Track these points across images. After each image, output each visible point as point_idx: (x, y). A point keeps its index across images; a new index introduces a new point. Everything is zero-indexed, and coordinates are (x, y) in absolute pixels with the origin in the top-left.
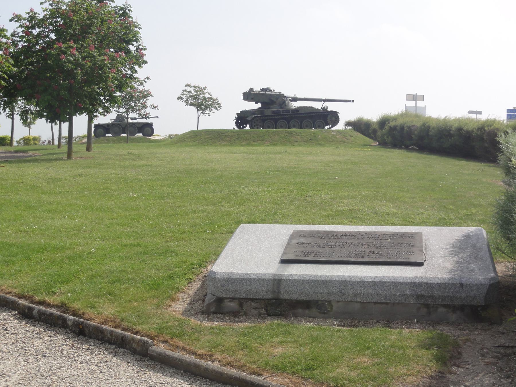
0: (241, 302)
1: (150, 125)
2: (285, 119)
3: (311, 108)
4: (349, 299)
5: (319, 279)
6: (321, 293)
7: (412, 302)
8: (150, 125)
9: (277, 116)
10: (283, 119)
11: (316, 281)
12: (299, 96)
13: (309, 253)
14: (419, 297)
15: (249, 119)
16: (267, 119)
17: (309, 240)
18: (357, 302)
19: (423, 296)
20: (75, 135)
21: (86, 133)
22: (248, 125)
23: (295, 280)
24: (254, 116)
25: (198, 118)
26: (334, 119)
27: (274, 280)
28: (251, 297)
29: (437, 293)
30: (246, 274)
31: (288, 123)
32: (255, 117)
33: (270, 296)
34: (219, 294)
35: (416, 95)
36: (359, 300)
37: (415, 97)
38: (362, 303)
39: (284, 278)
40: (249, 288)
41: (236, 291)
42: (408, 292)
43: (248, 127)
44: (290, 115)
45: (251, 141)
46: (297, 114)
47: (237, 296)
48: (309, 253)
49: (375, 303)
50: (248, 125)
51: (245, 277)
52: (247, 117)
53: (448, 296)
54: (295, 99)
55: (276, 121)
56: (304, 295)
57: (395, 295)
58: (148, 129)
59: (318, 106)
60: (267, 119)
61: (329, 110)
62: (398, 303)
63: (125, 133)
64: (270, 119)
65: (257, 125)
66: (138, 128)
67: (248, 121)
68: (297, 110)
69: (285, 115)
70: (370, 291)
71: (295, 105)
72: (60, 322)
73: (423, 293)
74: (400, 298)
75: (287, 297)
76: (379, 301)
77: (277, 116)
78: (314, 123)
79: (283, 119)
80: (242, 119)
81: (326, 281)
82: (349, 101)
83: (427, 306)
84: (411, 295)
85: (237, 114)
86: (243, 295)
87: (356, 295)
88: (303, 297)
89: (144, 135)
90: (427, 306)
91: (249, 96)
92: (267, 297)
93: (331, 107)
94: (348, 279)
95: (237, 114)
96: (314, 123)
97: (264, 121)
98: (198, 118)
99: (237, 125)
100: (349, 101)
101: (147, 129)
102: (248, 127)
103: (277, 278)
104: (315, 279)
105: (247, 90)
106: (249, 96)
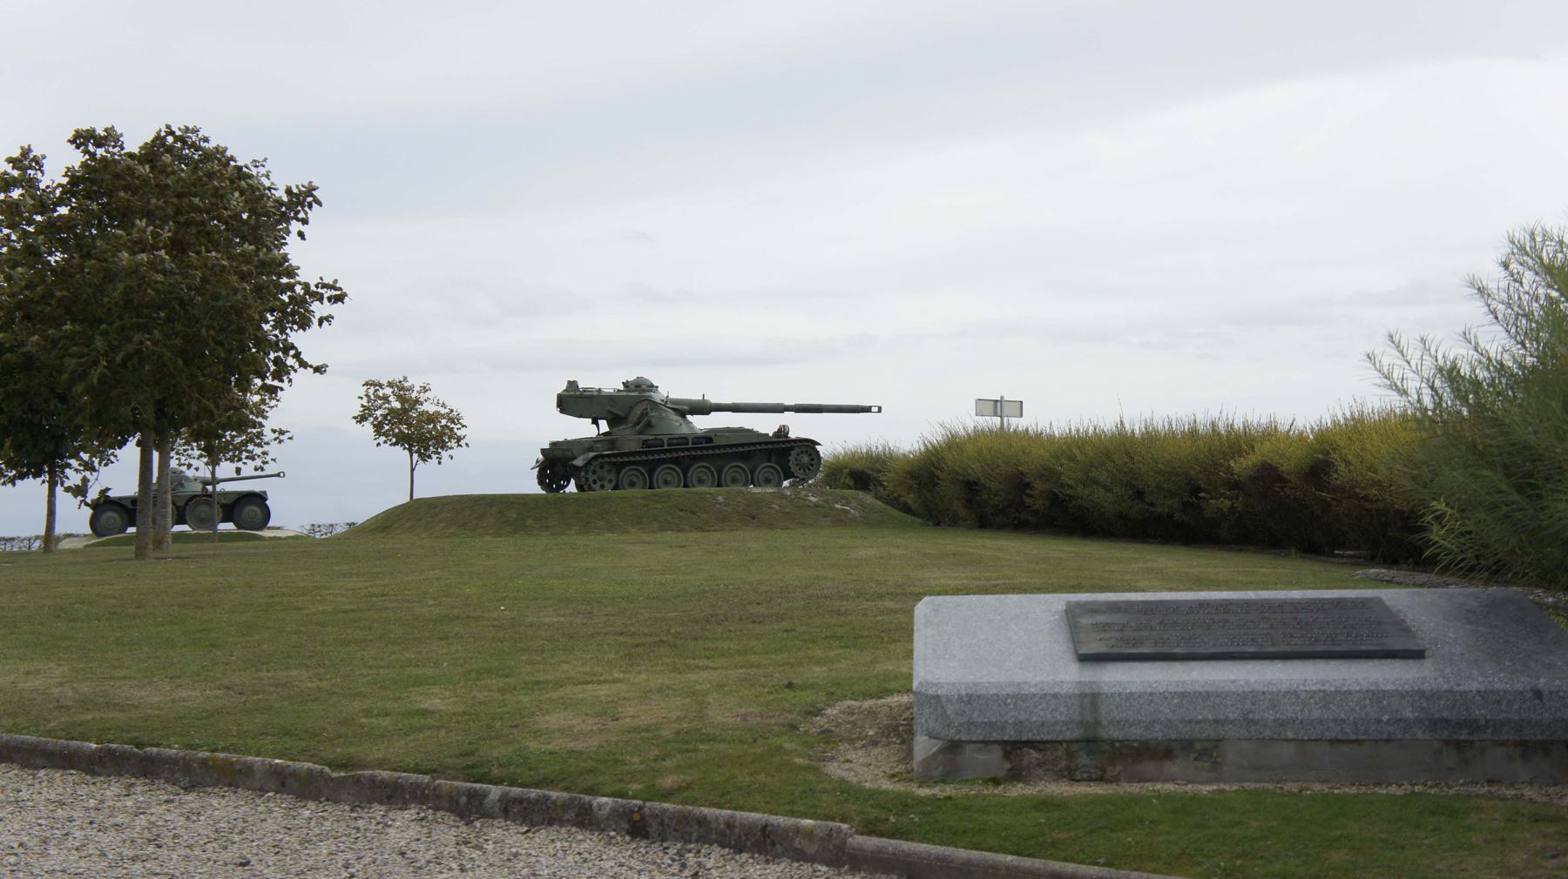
0: (1012, 748)
1: (259, 499)
2: (676, 461)
3: (741, 430)
4: (1268, 733)
5: (1189, 688)
6: (1199, 722)
7: (1420, 735)
8: (259, 499)
9: (652, 453)
10: (671, 461)
11: (1183, 695)
12: (714, 399)
13: (1137, 642)
14: (1436, 724)
15: (579, 462)
16: (629, 463)
17: (1118, 618)
18: (1287, 740)
19: (1447, 721)
20: (60, 529)
21: (42, 532)
22: (573, 482)
23: (1131, 694)
24: (592, 454)
25: (413, 470)
26: (806, 459)
27: (1083, 695)
28: (1030, 736)
29: (1479, 713)
30: (1011, 684)
31: (685, 473)
32: (595, 458)
33: (1077, 733)
34: (952, 733)
35: (1001, 401)
36: (1290, 735)
37: (997, 406)
38: (1299, 741)
39: (1106, 689)
40: (1023, 717)
41: (992, 725)
42: (1409, 714)
43: (572, 488)
44: (689, 449)
45: (582, 518)
46: (707, 449)
47: (995, 736)
48: (1137, 642)
49: (1332, 742)
50: (573, 482)
51: (1009, 690)
52: (574, 458)
53: (1509, 721)
54: (703, 408)
55: (652, 467)
56: (1157, 727)
57: (1379, 721)
58: (251, 510)
59: (766, 425)
60: (629, 463)
61: (792, 435)
62: (1388, 741)
63: (184, 522)
64: (634, 463)
65: (601, 479)
66: (223, 506)
67: (576, 467)
68: (708, 438)
69: (677, 451)
70: (1316, 714)
71: (700, 423)
72: (571, 815)
73: (1446, 714)
74: (1391, 728)
75: (1116, 734)
76: (1340, 736)
77: (652, 453)
78: (752, 473)
79: (671, 461)
80: (556, 463)
81: (1208, 694)
82: (867, 410)
83: (1459, 746)
84: (1418, 721)
85: (543, 451)
86: (1011, 734)
87: (1281, 725)
88: (1157, 734)
89: (238, 526)
90: (1459, 746)
91: (573, 401)
92: (1068, 736)
93: (800, 426)
94: (1260, 688)
95: (543, 451)
96: (752, 473)
97: (619, 467)
98: (413, 470)
99: (541, 482)
100: (867, 410)
101: (249, 509)
102: (572, 488)
103: (1087, 690)
104: (1180, 689)
105: (561, 387)
106: (573, 401)
